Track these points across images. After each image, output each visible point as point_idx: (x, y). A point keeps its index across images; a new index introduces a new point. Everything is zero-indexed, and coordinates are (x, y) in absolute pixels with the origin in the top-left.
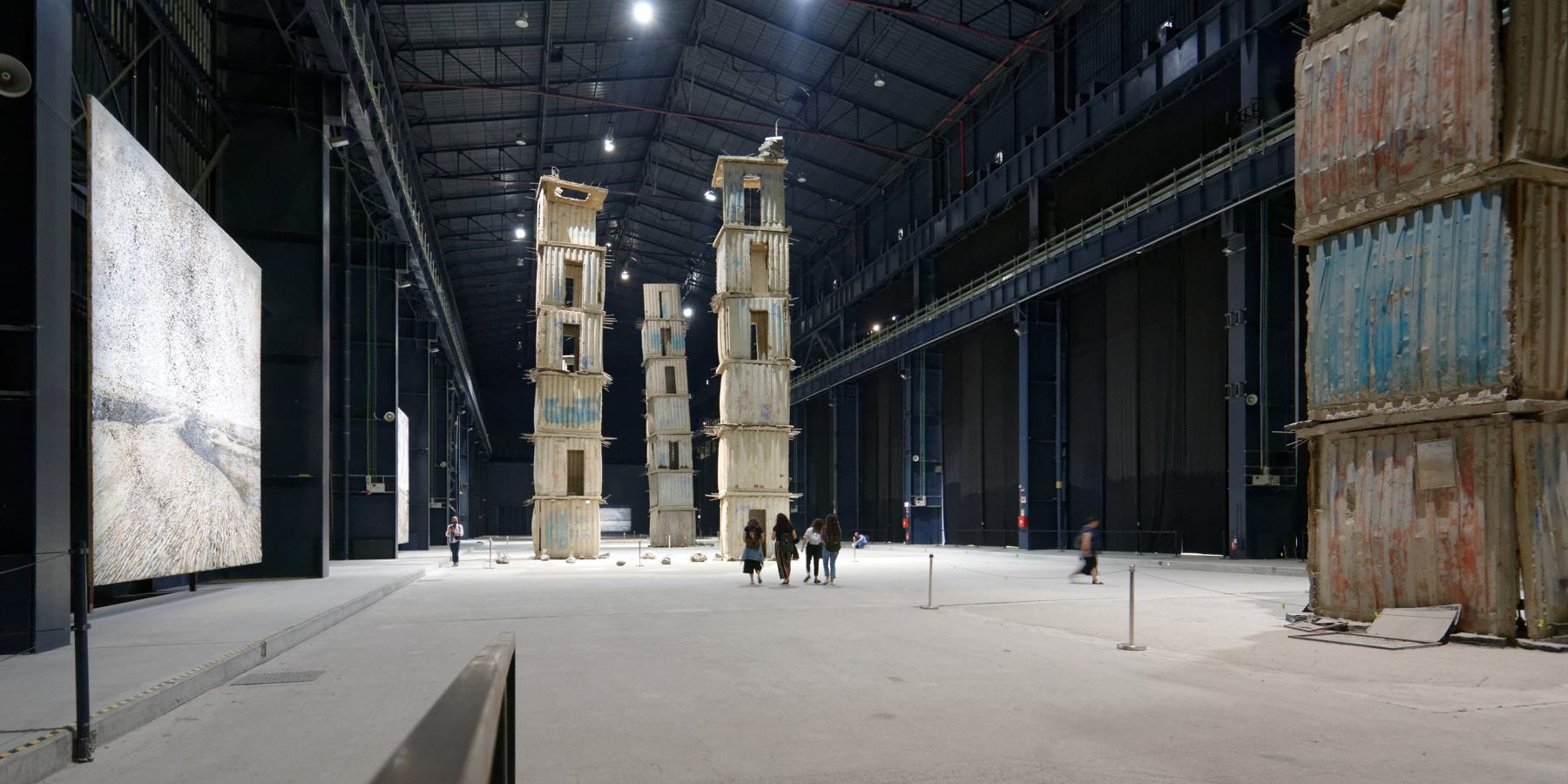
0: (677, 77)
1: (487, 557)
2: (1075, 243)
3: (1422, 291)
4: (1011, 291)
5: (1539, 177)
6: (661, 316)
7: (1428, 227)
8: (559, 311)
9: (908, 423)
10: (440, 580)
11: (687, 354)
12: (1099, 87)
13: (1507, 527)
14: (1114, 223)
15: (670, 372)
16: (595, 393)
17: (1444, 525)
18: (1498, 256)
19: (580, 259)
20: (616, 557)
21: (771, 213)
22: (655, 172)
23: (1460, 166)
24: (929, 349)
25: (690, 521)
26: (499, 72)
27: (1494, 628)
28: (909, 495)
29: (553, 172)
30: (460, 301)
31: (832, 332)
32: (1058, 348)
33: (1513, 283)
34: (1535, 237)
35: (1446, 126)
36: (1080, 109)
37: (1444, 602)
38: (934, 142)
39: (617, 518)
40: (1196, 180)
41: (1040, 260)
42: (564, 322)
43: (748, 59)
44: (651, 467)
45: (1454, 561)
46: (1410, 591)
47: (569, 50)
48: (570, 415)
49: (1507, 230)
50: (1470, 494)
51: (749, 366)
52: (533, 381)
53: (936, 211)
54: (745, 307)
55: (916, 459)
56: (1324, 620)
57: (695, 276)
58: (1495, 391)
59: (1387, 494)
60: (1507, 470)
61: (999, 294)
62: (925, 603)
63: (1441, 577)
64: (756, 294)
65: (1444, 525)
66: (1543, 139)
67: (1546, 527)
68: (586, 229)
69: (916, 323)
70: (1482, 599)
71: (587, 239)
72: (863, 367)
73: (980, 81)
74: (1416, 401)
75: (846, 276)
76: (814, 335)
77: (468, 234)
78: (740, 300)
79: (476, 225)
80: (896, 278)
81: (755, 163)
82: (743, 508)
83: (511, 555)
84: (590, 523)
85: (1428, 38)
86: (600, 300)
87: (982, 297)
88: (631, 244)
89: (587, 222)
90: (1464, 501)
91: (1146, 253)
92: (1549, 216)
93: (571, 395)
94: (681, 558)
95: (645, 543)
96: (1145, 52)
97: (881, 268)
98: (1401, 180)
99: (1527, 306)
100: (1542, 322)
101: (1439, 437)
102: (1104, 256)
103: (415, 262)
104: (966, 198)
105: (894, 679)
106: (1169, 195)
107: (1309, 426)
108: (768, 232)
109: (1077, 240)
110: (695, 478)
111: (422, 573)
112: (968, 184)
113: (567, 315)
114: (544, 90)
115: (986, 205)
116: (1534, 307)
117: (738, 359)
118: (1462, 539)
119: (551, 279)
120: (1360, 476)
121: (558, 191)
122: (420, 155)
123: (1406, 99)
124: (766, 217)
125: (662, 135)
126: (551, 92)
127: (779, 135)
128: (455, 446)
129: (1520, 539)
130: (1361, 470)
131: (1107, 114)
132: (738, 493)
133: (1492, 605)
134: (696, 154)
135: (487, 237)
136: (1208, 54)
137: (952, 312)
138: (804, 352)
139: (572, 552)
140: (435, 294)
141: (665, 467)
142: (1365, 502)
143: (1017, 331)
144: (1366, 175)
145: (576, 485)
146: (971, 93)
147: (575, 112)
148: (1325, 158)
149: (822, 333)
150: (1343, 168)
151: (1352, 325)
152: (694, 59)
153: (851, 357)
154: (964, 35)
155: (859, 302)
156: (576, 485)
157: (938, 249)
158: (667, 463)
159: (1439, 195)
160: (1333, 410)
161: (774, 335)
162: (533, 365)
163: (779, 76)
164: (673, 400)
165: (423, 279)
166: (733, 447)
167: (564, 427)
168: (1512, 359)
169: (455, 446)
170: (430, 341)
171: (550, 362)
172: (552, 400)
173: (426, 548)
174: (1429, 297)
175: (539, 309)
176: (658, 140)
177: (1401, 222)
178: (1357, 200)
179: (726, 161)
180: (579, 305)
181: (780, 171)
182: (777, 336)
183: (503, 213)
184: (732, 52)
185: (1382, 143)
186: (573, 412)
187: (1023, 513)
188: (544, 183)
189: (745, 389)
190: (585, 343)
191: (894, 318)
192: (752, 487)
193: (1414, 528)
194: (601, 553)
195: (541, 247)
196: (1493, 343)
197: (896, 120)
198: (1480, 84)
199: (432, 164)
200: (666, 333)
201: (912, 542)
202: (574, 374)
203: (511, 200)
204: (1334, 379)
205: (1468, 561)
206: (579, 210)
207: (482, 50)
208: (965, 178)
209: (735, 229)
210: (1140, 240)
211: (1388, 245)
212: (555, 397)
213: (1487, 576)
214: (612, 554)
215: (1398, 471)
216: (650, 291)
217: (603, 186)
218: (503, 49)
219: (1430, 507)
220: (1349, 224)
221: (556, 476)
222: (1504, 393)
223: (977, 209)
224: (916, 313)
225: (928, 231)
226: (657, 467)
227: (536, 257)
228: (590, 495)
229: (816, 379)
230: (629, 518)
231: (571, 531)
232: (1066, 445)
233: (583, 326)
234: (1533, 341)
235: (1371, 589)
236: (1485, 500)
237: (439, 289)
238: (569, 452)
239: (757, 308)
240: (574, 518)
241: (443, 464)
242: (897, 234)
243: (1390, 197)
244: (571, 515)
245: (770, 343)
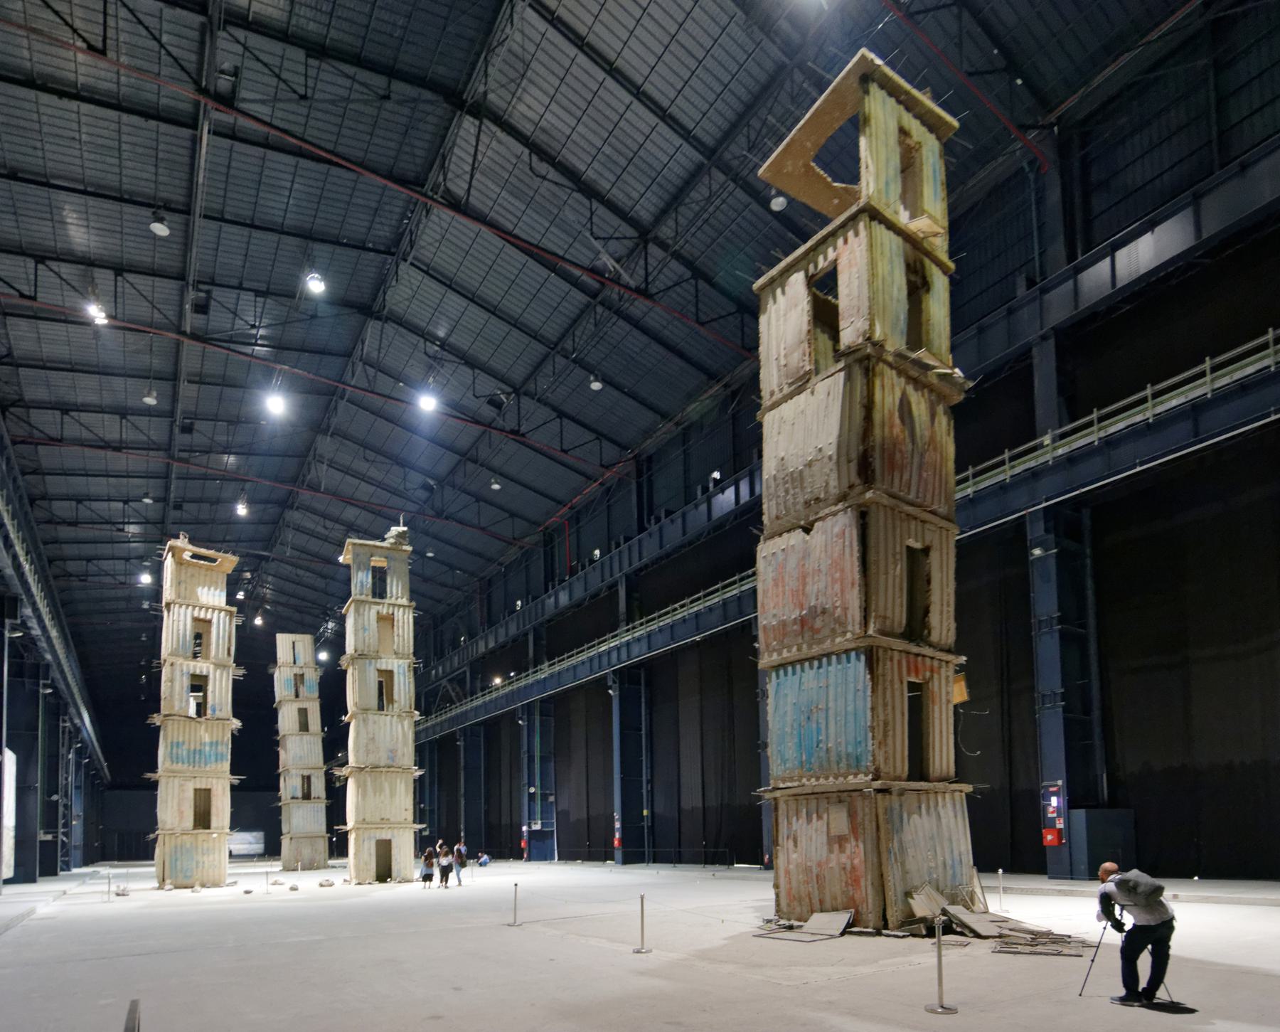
0: (310, 458)
1: (105, 888)
2: (652, 628)
3: (827, 710)
4: (605, 659)
5: (885, 645)
6: (295, 663)
7: (830, 668)
8: (186, 663)
9: (525, 761)
10: (54, 918)
11: (320, 697)
12: (668, 513)
13: (875, 860)
14: (679, 616)
15: (303, 713)
16: (223, 737)
17: (844, 859)
18: (865, 692)
19: (209, 617)
20: (244, 884)
21: (397, 589)
22: (290, 535)
23: (844, 633)
24: (542, 701)
25: (323, 846)
26: (124, 436)
27: (871, 924)
28: (526, 819)
29: (181, 537)
30: (76, 637)
31: (460, 681)
32: (643, 705)
33: (873, 709)
34: (884, 681)
35: (837, 607)
36: (654, 528)
37: (845, 908)
38: (544, 535)
39: (249, 841)
40: (735, 592)
41: (626, 639)
42: (191, 672)
43: (378, 451)
44: (283, 798)
45: (850, 881)
46: (828, 905)
47: (198, 425)
48: (196, 756)
49: (868, 677)
50: (857, 840)
51: (376, 717)
52: (158, 724)
53: (547, 591)
54: (372, 668)
55: (532, 790)
56: (782, 922)
57: (331, 625)
58: (866, 775)
59: (814, 837)
60: (874, 823)
61: (596, 662)
62: (511, 921)
63: (843, 892)
64: (383, 656)
65: (844, 859)
66: (888, 623)
67: (896, 859)
68: (216, 589)
69: (531, 680)
70: (865, 906)
71: (217, 598)
72: (487, 713)
73: (580, 494)
74: (827, 778)
75: (472, 635)
76: (444, 682)
77: (87, 576)
78: (367, 661)
79: (89, 513)
80: (514, 640)
81: (382, 547)
82: (370, 838)
83: (132, 886)
84: (216, 856)
85: (826, 552)
86: (229, 654)
87: (583, 663)
88: (265, 594)
89: (217, 583)
90: (854, 843)
91: (705, 640)
92: (892, 669)
93: (198, 739)
94: (308, 882)
95: (275, 866)
96: (699, 493)
97: (502, 631)
98: (815, 637)
99: (881, 724)
100: (891, 733)
101: (840, 801)
102: (672, 639)
103: (28, 611)
104: (570, 584)
105: (456, 989)
106: (716, 600)
107: (771, 791)
108: (394, 605)
109: (654, 626)
110: (327, 807)
111: (32, 911)
112: (573, 572)
113: (195, 667)
114: (172, 457)
115: (586, 590)
116: (886, 724)
117: (366, 710)
118: (853, 867)
119: (178, 634)
120: (799, 825)
121: (187, 556)
122: (32, 501)
123: (816, 587)
124: (391, 593)
125: (296, 505)
126: (180, 460)
127: (404, 526)
128: (69, 777)
129: (884, 867)
130: (800, 821)
131: (673, 534)
132: (365, 826)
133: (870, 910)
134: (329, 524)
135: (108, 580)
136: (742, 501)
137: (559, 673)
138: (427, 700)
139: (198, 883)
140: (49, 639)
141: (297, 798)
142: (802, 841)
143: (610, 692)
144: (796, 631)
145: (203, 819)
146: (574, 501)
147: (205, 477)
148: (775, 616)
149: (450, 681)
150: (784, 624)
151: (792, 726)
152: (325, 445)
153: (475, 703)
154: (566, 458)
155: (484, 658)
156: (203, 819)
157: (549, 621)
158: (299, 794)
159: (835, 649)
160: (784, 781)
161: (400, 690)
162: (158, 711)
163: (407, 470)
164: (306, 738)
165: (36, 626)
166: (361, 786)
167: (191, 768)
168: (873, 755)
169: (69, 777)
170: (41, 682)
171: (176, 708)
172: (178, 743)
173: (33, 881)
174: (831, 712)
175: (165, 661)
176: (292, 508)
177: (816, 663)
178: (792, 646)
179: (354, 544)
180: (207, 657)
181: (405, 556)
182: (402, 692)
183: (127, 559)
184: (365, 446)
185: (804, 612)
186: (200, 754)
187: (617, 835)
188: (171, 548)
189: (371, 736)
190: (214, 692)
191: (512, 674)
192: (378, 820)
193: (828, 861)
194: (229, 881)
195: (168, 605)
196: (863, 745)
197: (513, 515)
198: (853, 584)
199: (25, 421)
200: (299, 679)
201: (530, 859)
202: (202, 719)
203: (135, 548)
204: (784, 761)
205: (856, 881)
206: (209, 572)
207: (106, 416)
208: (571, 567)
209: (363, 601)
210: (698, 630)
211: (809, 675)
212: (181, 740)
213: (866, 892)
214: (241, 881)
215: (820, 823)
216: (283, 641)
217: (234, 554)
218: (129, 417)
219: (836, 847)
220: (789, 660)
221: (181, 813)
222: (870, 777)
223: (579, 593)
224: (530, 671)
225: (540, 606)
226: (289, 797)
227: (162, 611)
228: (217, 828)
229: (445, 721)
230: (262, 841)
231: (197, 863)
232: (650, 781)
233: (211, 676)
234: (886, 745)
235: (807, 900)
236: (864, 843)
237: (54, 633)
238: (196, 790)
239: (384, 667)
240: (200, 850)
241: (55, 797)
242: (515, 605)
243: (810, 647)
244: (197, 848)
245: (396, 697)
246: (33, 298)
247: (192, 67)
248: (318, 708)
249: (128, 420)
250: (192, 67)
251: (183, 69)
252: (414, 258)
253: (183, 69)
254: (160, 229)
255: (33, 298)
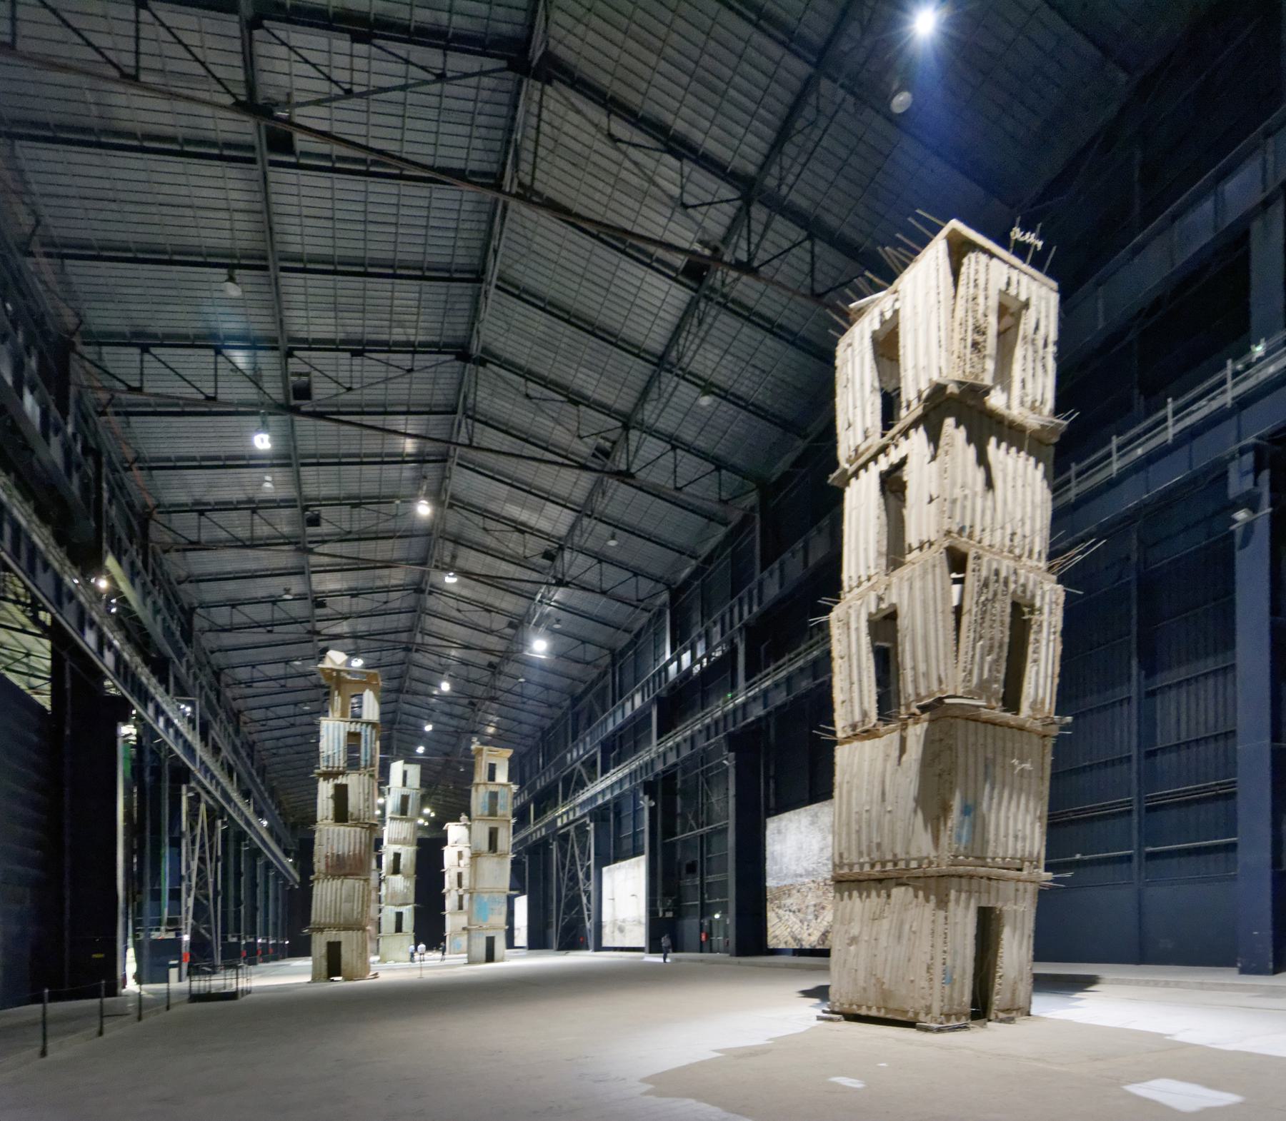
76: (578, 764)
246: (139, 390)
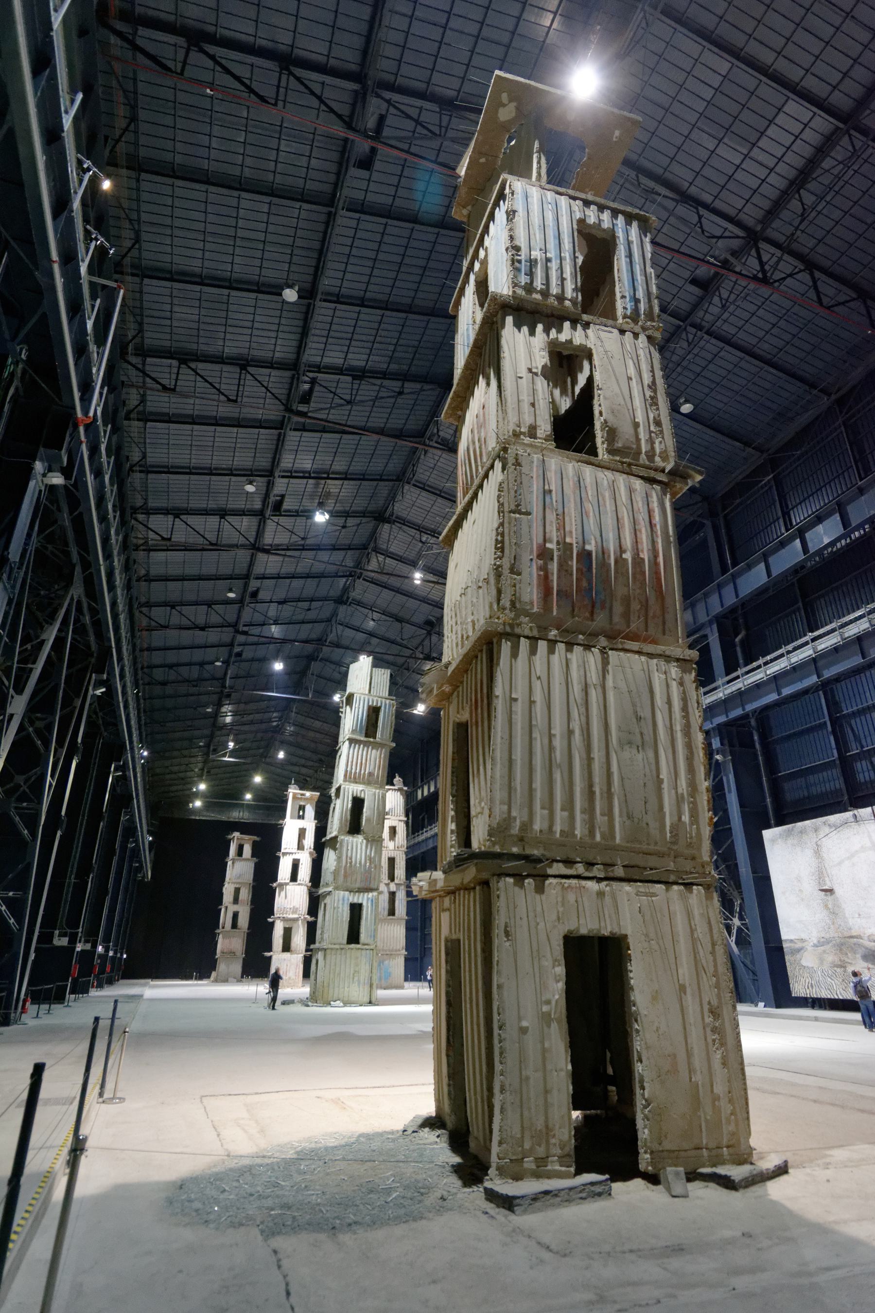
176: (345, 604)
247: (284, 402)
248: (314, 828)
249: (291, 73)
250: (283, 398)
251: (277, 398)
252: (417, 481)
253: (277, 398)
254: (250, 488)
255: (169, 539)
